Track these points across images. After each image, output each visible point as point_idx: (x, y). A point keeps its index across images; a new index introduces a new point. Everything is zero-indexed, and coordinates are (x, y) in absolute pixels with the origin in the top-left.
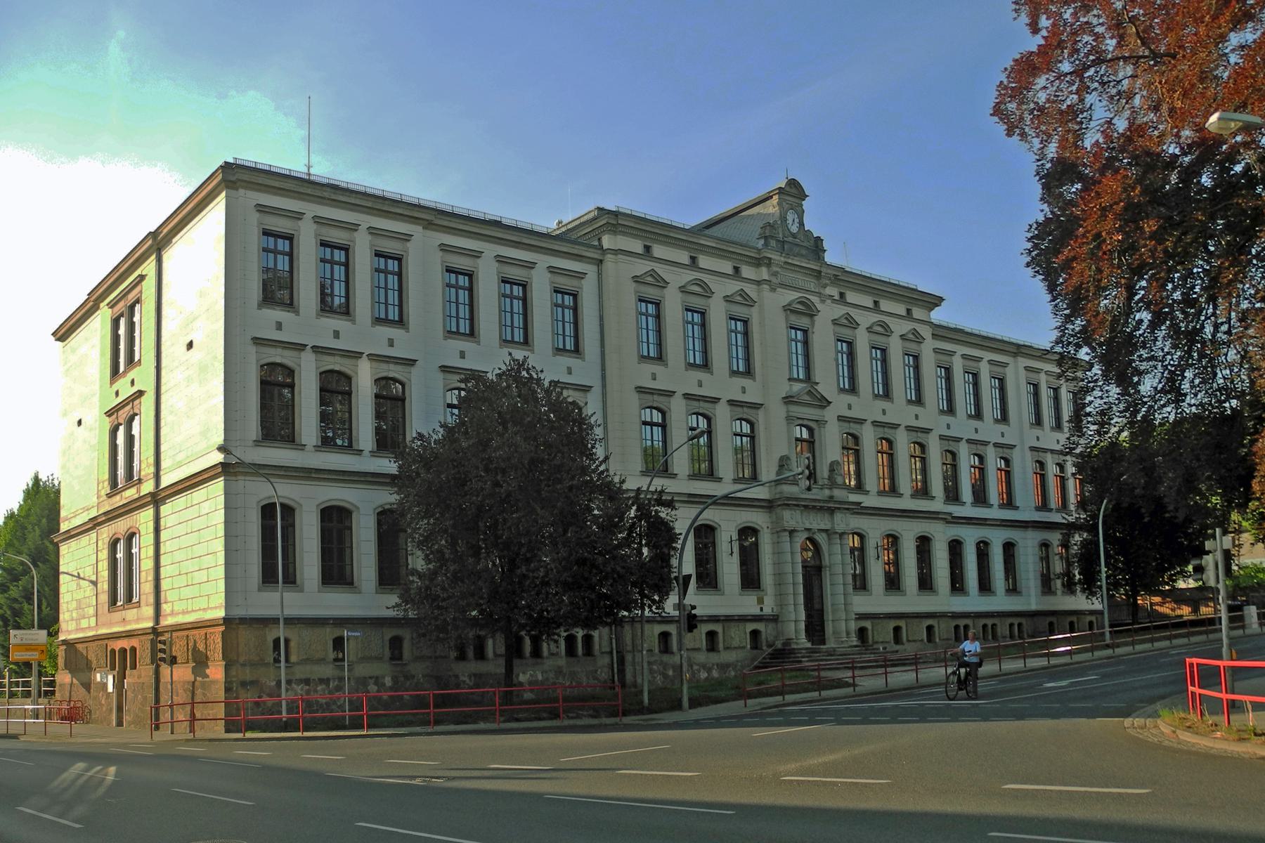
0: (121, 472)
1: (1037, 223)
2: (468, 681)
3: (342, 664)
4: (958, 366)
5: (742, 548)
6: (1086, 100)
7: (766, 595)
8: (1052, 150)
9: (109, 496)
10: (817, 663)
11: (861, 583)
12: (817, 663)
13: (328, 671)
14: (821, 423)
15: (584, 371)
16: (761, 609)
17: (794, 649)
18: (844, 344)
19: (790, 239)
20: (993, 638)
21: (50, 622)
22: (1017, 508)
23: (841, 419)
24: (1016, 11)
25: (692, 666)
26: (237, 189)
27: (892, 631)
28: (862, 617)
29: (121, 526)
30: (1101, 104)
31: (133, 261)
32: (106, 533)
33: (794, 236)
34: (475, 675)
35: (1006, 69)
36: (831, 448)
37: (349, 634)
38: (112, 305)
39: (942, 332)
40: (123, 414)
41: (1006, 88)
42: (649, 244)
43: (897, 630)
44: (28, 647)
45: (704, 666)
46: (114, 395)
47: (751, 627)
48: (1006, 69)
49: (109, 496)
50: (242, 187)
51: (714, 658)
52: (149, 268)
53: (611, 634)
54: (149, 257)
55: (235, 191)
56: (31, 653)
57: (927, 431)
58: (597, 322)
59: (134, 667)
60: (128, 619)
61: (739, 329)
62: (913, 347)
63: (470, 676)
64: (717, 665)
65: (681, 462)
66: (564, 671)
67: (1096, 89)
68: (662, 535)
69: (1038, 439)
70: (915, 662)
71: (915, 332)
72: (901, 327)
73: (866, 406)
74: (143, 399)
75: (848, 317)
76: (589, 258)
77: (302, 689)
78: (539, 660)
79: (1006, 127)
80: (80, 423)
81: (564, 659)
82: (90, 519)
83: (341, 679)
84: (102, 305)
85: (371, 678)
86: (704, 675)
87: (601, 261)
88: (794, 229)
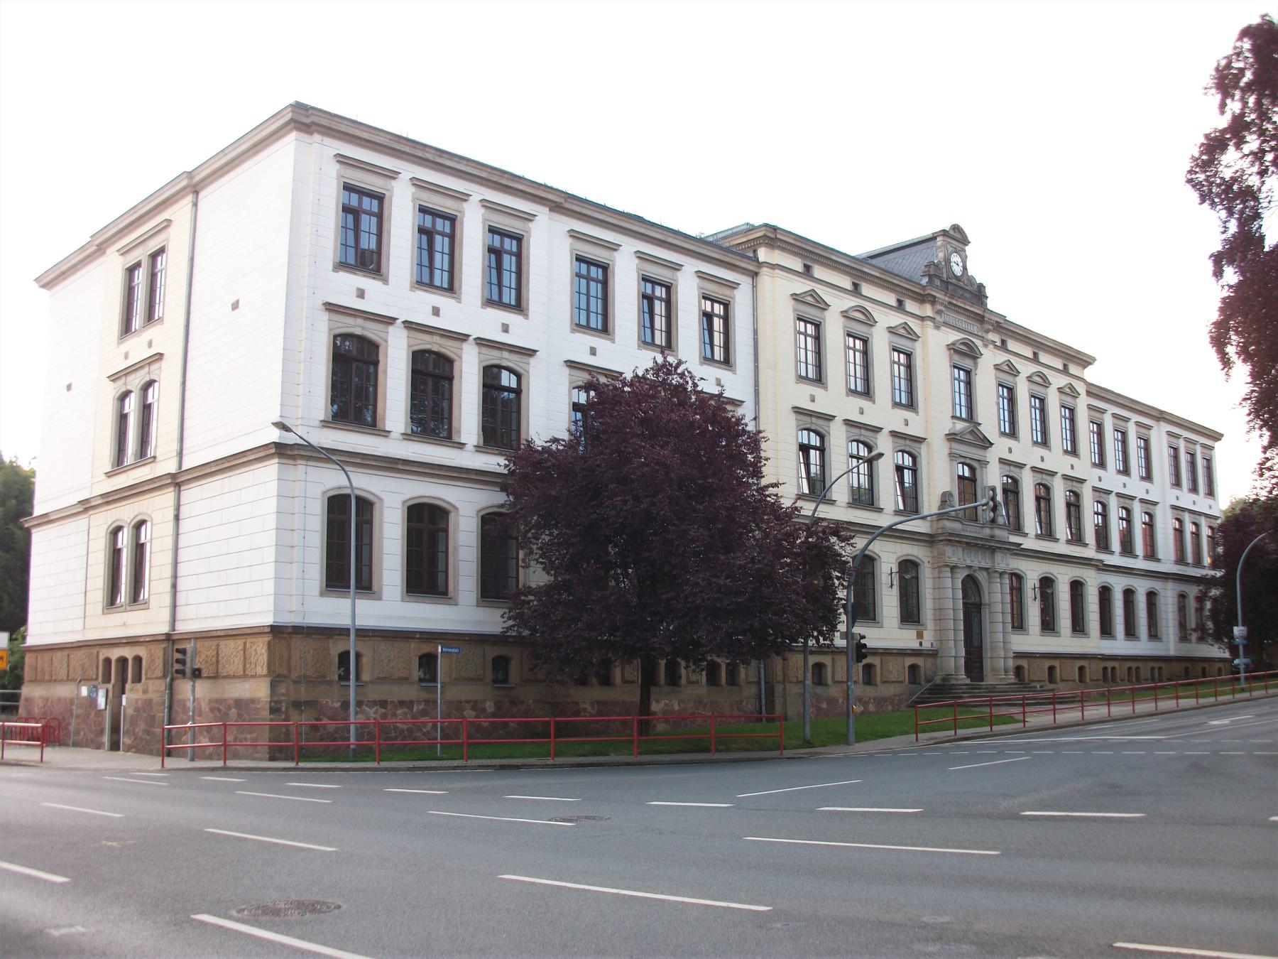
5: (901, 579)
9: (109, 475)
13: (411, 692)
14: (984, 463)
17: (953, 684)
22: (1158, 560)
29: (126, 513)
32: (103, 520)
34: (598, 702)
38: (124, 252)
39: (1095, 392)
47: (909, 661)
49: (109, 475)
51: (870, 692)
52: (180, 213)
54: (183, 197)
57: (1082, 481)
59: (138, 679)
63: (592, 704)
64: (874, 699)
71: (1071, 387)
73: (1024, 451)
74: (164, 363)
77: (376, 713)
80: (69, 387)
82: (79, 502)
85: (468, 702)
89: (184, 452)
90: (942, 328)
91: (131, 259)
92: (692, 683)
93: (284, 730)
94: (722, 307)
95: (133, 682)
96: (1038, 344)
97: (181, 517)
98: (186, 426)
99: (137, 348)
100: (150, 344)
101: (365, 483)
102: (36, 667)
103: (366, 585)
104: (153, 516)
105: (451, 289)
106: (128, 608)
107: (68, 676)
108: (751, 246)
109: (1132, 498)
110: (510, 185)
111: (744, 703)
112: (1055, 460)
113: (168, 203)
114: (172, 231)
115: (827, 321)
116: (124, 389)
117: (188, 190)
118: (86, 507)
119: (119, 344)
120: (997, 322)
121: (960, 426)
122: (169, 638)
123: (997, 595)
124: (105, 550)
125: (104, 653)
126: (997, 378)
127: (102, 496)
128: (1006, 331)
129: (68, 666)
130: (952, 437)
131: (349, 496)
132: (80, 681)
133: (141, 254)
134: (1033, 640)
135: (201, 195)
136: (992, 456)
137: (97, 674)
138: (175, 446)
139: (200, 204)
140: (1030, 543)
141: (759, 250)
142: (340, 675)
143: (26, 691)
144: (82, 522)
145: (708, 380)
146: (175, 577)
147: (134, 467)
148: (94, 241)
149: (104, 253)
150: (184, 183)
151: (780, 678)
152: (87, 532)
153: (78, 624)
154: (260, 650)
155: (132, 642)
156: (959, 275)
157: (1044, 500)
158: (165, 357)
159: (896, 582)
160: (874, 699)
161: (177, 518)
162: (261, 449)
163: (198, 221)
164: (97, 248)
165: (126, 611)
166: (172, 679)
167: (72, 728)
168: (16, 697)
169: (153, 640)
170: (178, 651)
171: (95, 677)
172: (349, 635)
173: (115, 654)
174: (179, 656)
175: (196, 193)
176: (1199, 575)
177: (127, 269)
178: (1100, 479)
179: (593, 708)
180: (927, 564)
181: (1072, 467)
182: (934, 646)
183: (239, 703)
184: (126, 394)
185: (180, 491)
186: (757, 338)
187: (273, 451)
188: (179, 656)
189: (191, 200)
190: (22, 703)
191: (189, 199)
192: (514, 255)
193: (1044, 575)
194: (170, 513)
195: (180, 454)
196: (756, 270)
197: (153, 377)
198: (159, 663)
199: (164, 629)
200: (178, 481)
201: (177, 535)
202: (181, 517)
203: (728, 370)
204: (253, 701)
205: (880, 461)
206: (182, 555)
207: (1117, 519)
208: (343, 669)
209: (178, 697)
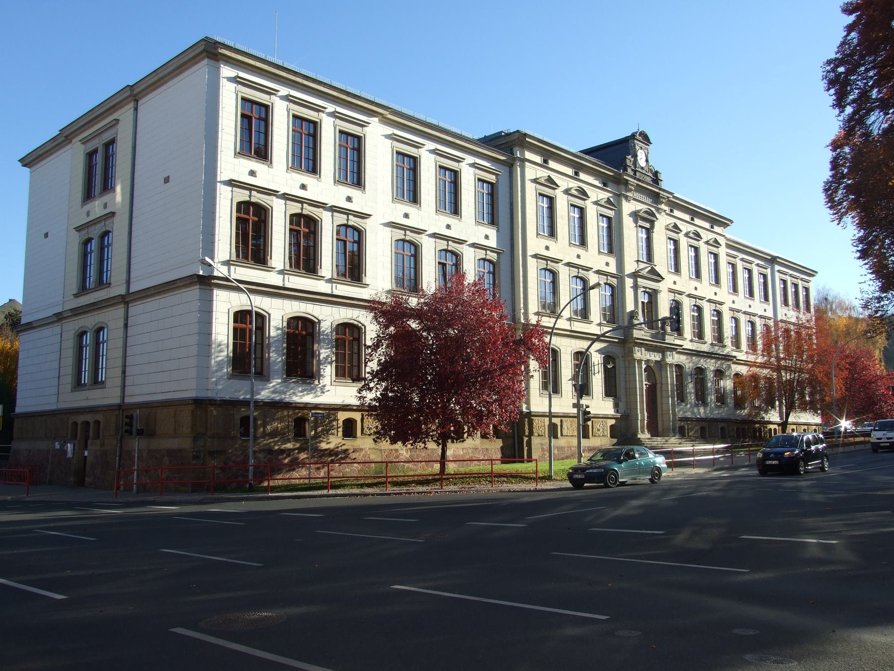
0: (92, 271)
4: (740, 266)
5: (606, 369)
7: (621, 401)
9: (76, 296)
11: (682, 397)
23: (671, 291)
25: (571, 448)
29: (89, 321)
31: (111, 106)
32: (72, 327)
33: (642, 168)
38: (84, 142)
39: (733, 246)
46: (85, 215)
49: (76, 296)
52: (125, 115)
54: (126, 104)
57: (721, 304)
58: (508, 205)
59: (97, 436)
60: (632, 312)
62: (714, 250)
71: (716, 241)
72: (706, 236)
73: (685, 283)
74: (116, 219)
81: (479, 440)
82: (54, 314)
84: (74, 141)
87: (512, 165)
90: (632, 201)
91: (91, 146)
96: (694, 213)
98: (136, 182)
99: (97, 208)
100: (105, 206)
101: (261, 303)
104: (108, 324)
105: (314, 169)
106: (90, 387)
108: (509, 146)
112: (705, 289)
113: (116, 107)
114: (120, 126)
116: (86, 237)
117: (131, 98)
118: (59, 317)
119: (82, 206)
124: (74, 348)
125: (72, 419)
126: (666, 235)
127: (71, 310)
128: (676, 205)
131: (249, 312)
132: (54, 439)
133: (98, 143)
135: (140, 103)
139: (140, 109)
141: (514, 149)
142: (241, 433)
143: (15, 445)
144: (57, 328)
146: (124, 366)
147: (95, 290)
148: (63, 133)
149: (71, 142)
150: (128, 93)
151: (527, 434)
152: (60, 335)
153: (54, 399)
154: (186, 416)
158: (116, 215)
161: (126, 326)
162: (187, 279)
163: (138, 121)
165: (89, 390)
166: (122, 437)
168: (8, 450)
169: (109, 408)
170: (127, 417)
172: (249, 405)
173: (81, 419)
175: (137, 101)
177: (86, 154)
178: (733, 302)
180: (621, 358)
181: (716, 294)
182: (626, 412)
183: (170, 452)
184: (89, 240)
185: (128, 307)
186: (513, 208)
187: (196, 280)
189: (133, 106)
191: (132, 105)
192: (311, 136)
194: (121, 323)
195: (128, 282)
196: (512, 162)
197: (108, 229)
199: (117, 401)
200: (126, 300)
202: (129, 325)
204: (180, 451)
206: (129, 351)
208: (243, 428)
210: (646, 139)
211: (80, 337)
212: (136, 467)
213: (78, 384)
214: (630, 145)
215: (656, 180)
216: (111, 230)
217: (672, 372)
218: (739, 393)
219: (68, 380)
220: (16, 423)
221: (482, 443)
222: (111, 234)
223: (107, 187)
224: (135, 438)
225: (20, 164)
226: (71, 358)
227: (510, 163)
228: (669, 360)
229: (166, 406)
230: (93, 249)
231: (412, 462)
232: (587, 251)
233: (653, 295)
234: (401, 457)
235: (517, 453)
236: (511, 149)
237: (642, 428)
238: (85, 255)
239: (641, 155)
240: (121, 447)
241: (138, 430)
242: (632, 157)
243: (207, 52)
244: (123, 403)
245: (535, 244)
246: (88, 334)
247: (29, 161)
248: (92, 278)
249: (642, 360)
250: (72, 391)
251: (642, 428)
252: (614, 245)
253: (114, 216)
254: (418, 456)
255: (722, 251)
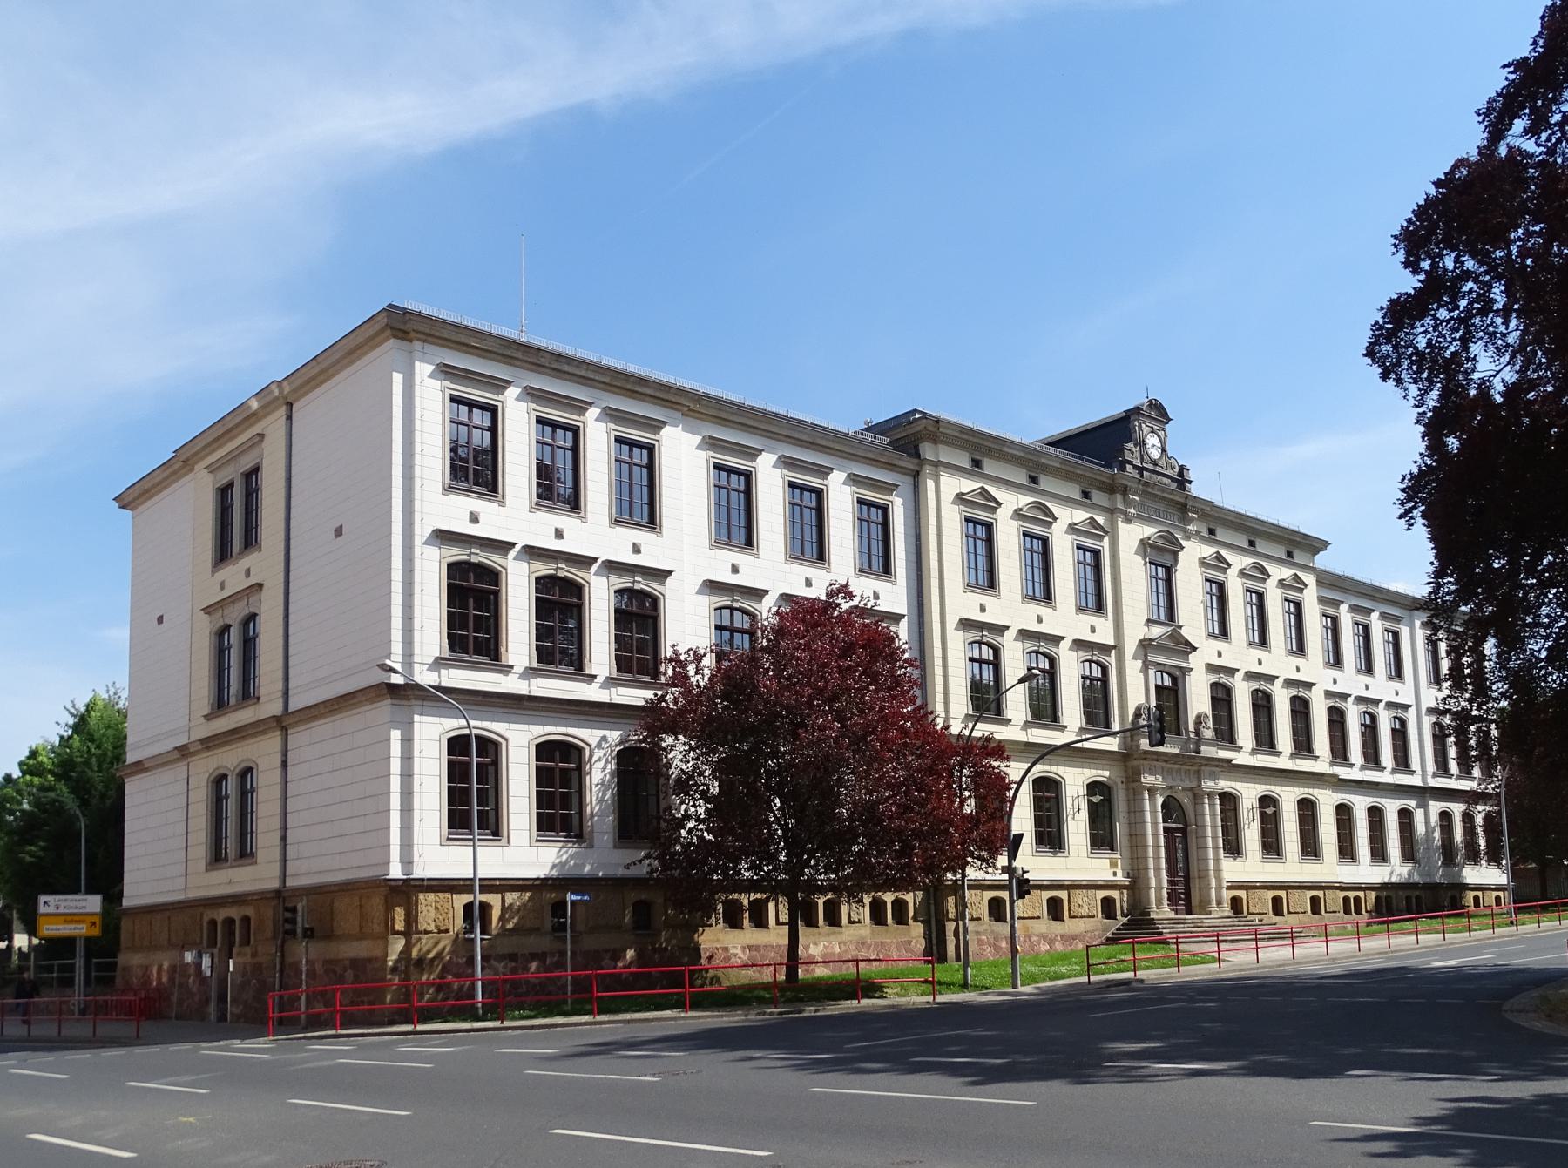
1: (1411, 474)
2: (740, 954)
3: (562, 934)
6: (1471, 349)
8: (1433, 398)
9: (208, 718)
10: (1175, 935)
12: (1175, 935)
13: (544, 943)
14: (1185, 671)
15: (892, 596)
16: (1115, 874)
17: (1153, 919)
18: (1214, 585)
19: (1150, 466)
20: (1387, 911)
21: (107, 879)
23: (1212, 668)
24: (1395, 246)
25: (1030, 938)
26: (411, 341)
27: (1270, 901)
28: (1234, 886)
30: (1486, 354)
32: (204, 767)
33: (1155, 463)
34: (750, 947)
35: (1382, 308)
36: (1198, 701)
37: (574, 898)
38: (213, 469)
39: (1334, 584)
40: (235, 615)
41: (1382, 328)
42: (979, 458)
43: (1276, 901)
44: (69, 918)
45: (1045, 938)
47: (1101, 894)
48: (1382, 308)
50: (419, 340)
51: (1057, 927)
53: (929, 899)
55: (408, 343)
56: (73, 926)
57: (1309, 686)
59: (246, 941)
61: (1088, 560)
63: (743, 948)
64: (1062, 936)
65: (1017, 703)
66: (869, 941)
67: (1481, 338)
68: (995, 794)
69: (1298, 669)
70: (1292, 936)
73: (1238, 653)
74: (265, 593)
75: (1219, 558)
76: (902, 467)
77: (505, 967)
78: (836, 929)
79: (1380, 370)
80: (160, 620)
82: (176, 748)
83: (563, 953)
85: (607, 951)
86: (1044, 947)
87: (918, 473)
88: (1155, 454)
89: (290, 693)
92: (854, 922)
93: (404, 990)
94: (880, 511)
95: (240, 945)
96: (1253, 532)
97: (289, 763)
98: (292, 535)
99: (234, 576)
100: (248, 573)
102: (134, 933)
103: (492, 826)
105: (574, 503)
107: (169, 940)
109: (1376, 702)
110: (636, 389)
111: (913, 944)
112: (1278, 661)
115: (998, 521)
116: (221, 623)
118: (183, 752)
119: (213, 573)
120: (1202, 509)
121: (1157, 631)
122: (279, 894)
123: (1211, 817)
125: (209, 915)
128: (1217, 521)
129: (169, 931)
130: (1146, 645)
131: (467, 737)
132: (183, 947)
133: (233, 473)
134: (1251, 867)
136: (1196, 661)
137: (202, 937)
138: (280, 686)
140: (1243, 757)
143: (123, 959)
144: (180, 770)
145: (865, 588)
146: (284, 828)
147: (238, 707)
149: (192, 469)
151: (952, 915)
155: (238, 899)
156: (1156, 458)
157: (1262, 705)
158: (265, 588)
159: (1257, 816)
160: (1062, 936)
161: (285, 764)
164: (182, 463)
166: (283, 942)
167: (174, 999)
169: (262, 897)
170: (286, 909)
171: (198, 941)
173: (221, 915)
174: (288, 915)
176: (1468, 789)
177: (218, 488)
179: (744, 952)
181: (1298, 669)
184: (227, 628)
188: (288, 915)
190: (119, 973)
193: (1226, 790)
196: (917, 468)
197: (253, 610)
198: (269, 924)
199: (276, 884)
201: (285, 782)
203: (887, 581)
205: (1021, 675)
207: (992, 730)
209: (289, 960)
210: (1158, 414)
211: (242, 777)
212: (304, 988)
213: (217, 857)
214: (1131, 426)
215: (1182, 480)
216: (257, 612)
217: (1212, 805)
218: (651, 882)
219: (200, 852)
220: (126, 925)
221: (873, 932)
222: (258, 617)
223: (251, 540)
224: (302, 942)
225: (117, 505)
226: (205, 817)
227: (912, 470)
228: (1208, 785)
229: (348, 890)
230: (231, 642)
231: (752, 966)
232: (1054, 608)
233: (1178, 678)
234: (733, 959)
235: (935, 948)
236: (916, 447)
237: (1159, 901)
238: (221, 651)
239: (1152, 440)
240: (283, 956)
241: (305, 930)
242: (1136, 445)
243: (392, 328)
244: (285, 886)
245: (961, 602)
246: (229, 778)
247: (126, 501)
248: (231, 689)
249: (1157, 789)
250: (207, 870)
251: (1159, 901)
252: (1095, 599)
253: (261, 590)
254: (762, 957)
255: (1310, 598)
